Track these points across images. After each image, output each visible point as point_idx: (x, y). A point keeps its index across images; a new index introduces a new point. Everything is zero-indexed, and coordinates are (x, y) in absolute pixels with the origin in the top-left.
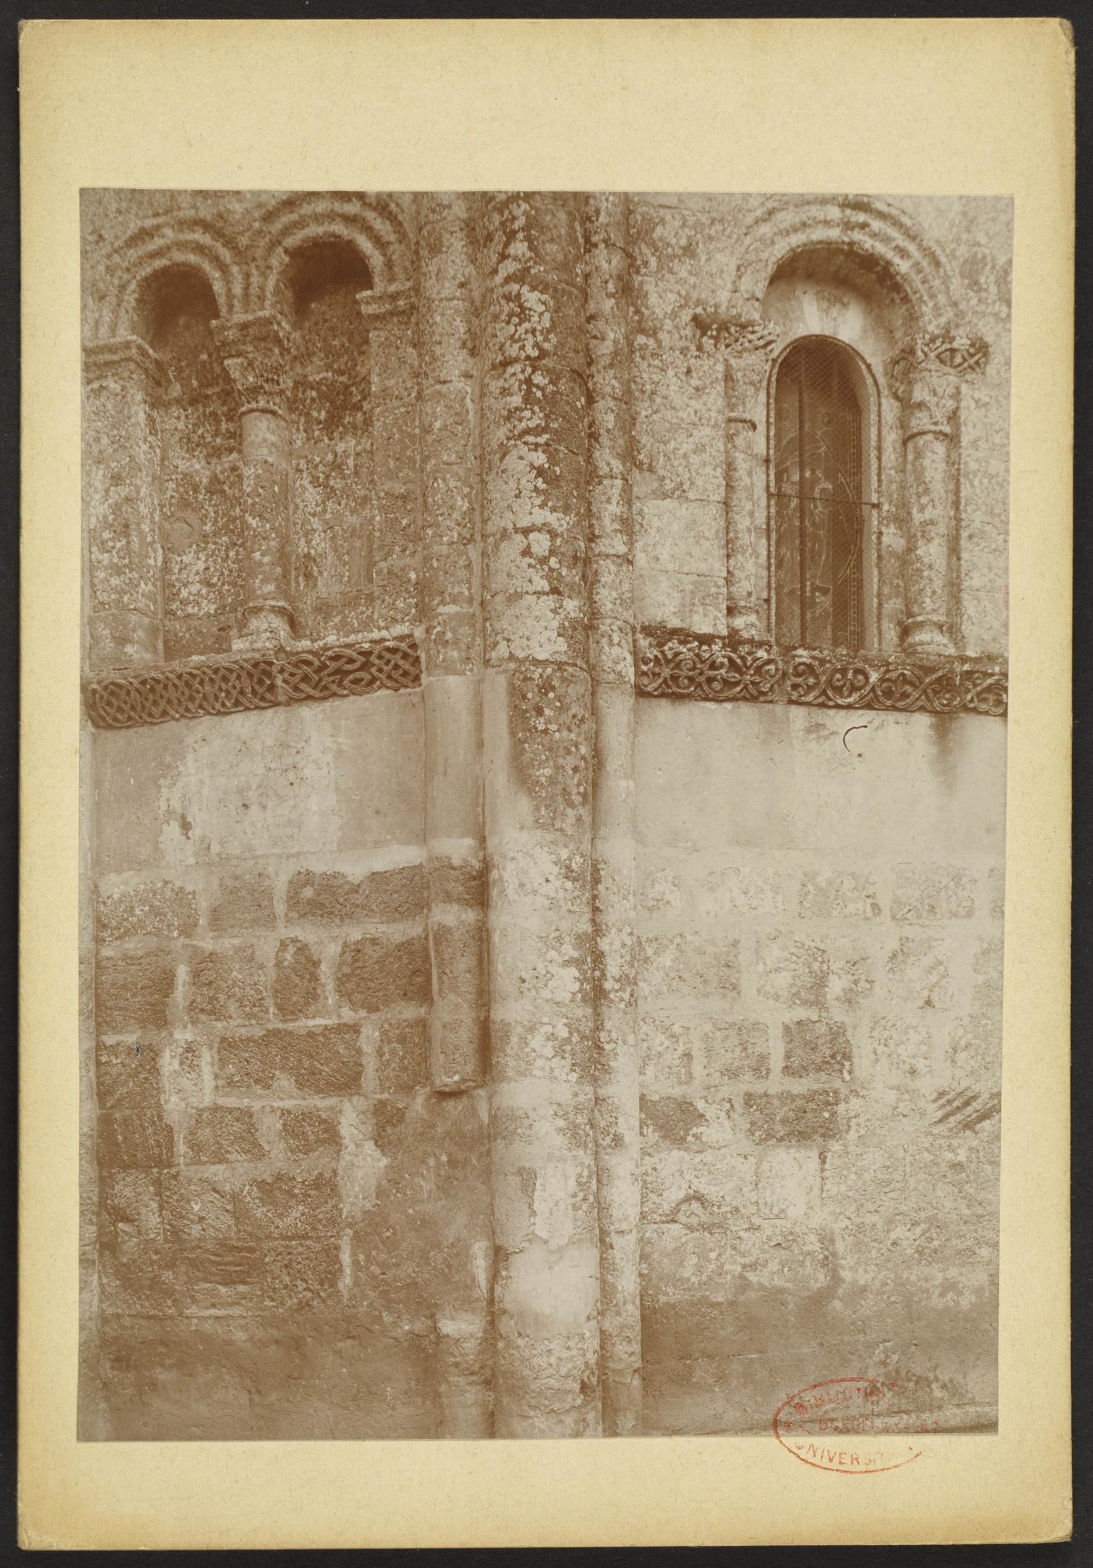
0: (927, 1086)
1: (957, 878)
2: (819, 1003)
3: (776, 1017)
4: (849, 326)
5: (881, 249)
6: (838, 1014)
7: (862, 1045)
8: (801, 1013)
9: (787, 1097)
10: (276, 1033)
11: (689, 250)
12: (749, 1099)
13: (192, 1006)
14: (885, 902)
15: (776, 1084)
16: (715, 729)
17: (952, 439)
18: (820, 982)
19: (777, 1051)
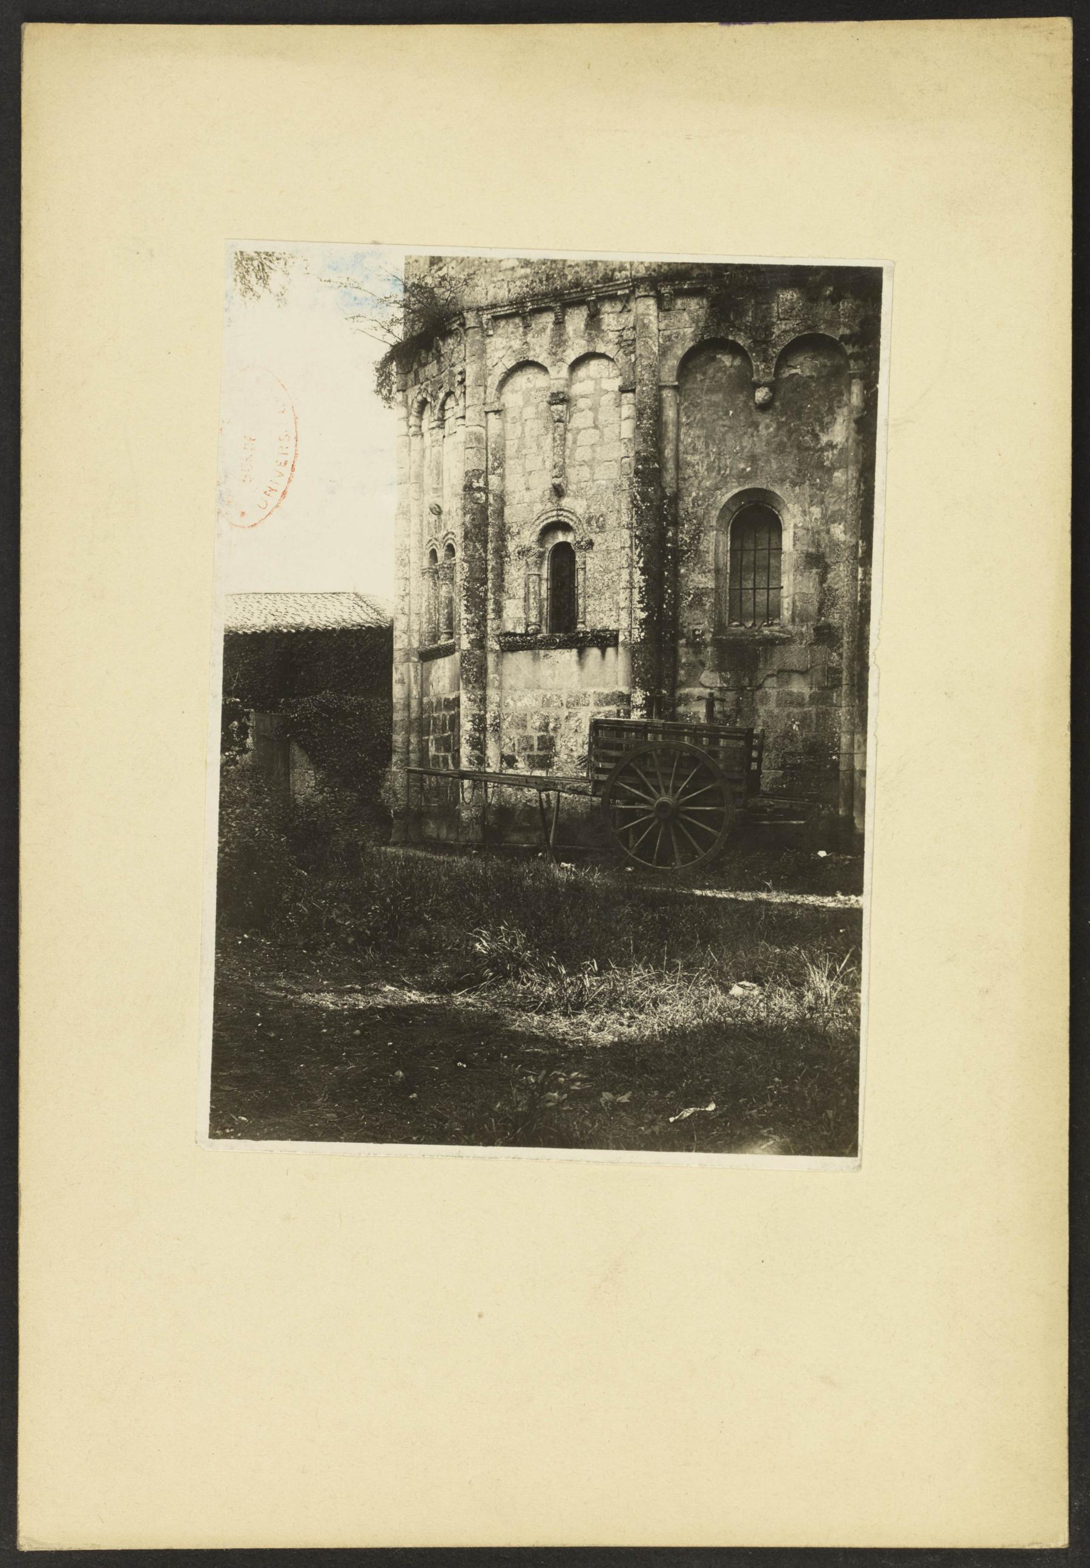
0: (575, 754)
1: (585, 695)
2: (547, 731)
3: (536, 735)
4: (561, 537)
5: (566, 520)
6: (552, 734)
7: (559, 742)
8: (542, 733)
9: (538, 756)
10: (693, 500)
11: (518, 533)
12: (529, 756)
13: (841, 672)
14: (565, 703)
15: (535, 752)
16: (520, 660)
17: (584, 569)
18: (547, 725)
19: (536, 743)
